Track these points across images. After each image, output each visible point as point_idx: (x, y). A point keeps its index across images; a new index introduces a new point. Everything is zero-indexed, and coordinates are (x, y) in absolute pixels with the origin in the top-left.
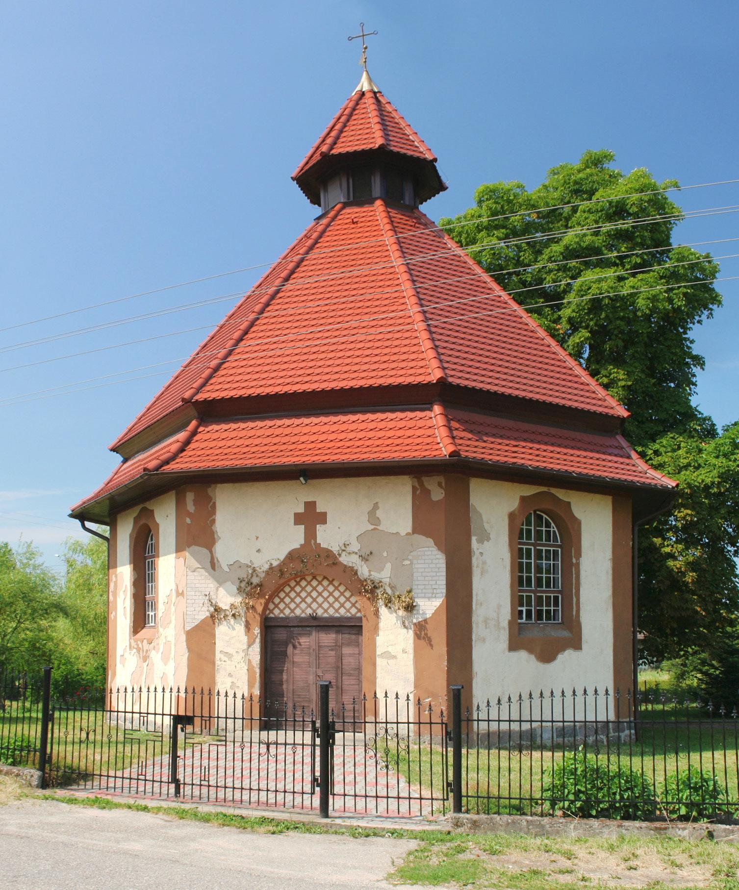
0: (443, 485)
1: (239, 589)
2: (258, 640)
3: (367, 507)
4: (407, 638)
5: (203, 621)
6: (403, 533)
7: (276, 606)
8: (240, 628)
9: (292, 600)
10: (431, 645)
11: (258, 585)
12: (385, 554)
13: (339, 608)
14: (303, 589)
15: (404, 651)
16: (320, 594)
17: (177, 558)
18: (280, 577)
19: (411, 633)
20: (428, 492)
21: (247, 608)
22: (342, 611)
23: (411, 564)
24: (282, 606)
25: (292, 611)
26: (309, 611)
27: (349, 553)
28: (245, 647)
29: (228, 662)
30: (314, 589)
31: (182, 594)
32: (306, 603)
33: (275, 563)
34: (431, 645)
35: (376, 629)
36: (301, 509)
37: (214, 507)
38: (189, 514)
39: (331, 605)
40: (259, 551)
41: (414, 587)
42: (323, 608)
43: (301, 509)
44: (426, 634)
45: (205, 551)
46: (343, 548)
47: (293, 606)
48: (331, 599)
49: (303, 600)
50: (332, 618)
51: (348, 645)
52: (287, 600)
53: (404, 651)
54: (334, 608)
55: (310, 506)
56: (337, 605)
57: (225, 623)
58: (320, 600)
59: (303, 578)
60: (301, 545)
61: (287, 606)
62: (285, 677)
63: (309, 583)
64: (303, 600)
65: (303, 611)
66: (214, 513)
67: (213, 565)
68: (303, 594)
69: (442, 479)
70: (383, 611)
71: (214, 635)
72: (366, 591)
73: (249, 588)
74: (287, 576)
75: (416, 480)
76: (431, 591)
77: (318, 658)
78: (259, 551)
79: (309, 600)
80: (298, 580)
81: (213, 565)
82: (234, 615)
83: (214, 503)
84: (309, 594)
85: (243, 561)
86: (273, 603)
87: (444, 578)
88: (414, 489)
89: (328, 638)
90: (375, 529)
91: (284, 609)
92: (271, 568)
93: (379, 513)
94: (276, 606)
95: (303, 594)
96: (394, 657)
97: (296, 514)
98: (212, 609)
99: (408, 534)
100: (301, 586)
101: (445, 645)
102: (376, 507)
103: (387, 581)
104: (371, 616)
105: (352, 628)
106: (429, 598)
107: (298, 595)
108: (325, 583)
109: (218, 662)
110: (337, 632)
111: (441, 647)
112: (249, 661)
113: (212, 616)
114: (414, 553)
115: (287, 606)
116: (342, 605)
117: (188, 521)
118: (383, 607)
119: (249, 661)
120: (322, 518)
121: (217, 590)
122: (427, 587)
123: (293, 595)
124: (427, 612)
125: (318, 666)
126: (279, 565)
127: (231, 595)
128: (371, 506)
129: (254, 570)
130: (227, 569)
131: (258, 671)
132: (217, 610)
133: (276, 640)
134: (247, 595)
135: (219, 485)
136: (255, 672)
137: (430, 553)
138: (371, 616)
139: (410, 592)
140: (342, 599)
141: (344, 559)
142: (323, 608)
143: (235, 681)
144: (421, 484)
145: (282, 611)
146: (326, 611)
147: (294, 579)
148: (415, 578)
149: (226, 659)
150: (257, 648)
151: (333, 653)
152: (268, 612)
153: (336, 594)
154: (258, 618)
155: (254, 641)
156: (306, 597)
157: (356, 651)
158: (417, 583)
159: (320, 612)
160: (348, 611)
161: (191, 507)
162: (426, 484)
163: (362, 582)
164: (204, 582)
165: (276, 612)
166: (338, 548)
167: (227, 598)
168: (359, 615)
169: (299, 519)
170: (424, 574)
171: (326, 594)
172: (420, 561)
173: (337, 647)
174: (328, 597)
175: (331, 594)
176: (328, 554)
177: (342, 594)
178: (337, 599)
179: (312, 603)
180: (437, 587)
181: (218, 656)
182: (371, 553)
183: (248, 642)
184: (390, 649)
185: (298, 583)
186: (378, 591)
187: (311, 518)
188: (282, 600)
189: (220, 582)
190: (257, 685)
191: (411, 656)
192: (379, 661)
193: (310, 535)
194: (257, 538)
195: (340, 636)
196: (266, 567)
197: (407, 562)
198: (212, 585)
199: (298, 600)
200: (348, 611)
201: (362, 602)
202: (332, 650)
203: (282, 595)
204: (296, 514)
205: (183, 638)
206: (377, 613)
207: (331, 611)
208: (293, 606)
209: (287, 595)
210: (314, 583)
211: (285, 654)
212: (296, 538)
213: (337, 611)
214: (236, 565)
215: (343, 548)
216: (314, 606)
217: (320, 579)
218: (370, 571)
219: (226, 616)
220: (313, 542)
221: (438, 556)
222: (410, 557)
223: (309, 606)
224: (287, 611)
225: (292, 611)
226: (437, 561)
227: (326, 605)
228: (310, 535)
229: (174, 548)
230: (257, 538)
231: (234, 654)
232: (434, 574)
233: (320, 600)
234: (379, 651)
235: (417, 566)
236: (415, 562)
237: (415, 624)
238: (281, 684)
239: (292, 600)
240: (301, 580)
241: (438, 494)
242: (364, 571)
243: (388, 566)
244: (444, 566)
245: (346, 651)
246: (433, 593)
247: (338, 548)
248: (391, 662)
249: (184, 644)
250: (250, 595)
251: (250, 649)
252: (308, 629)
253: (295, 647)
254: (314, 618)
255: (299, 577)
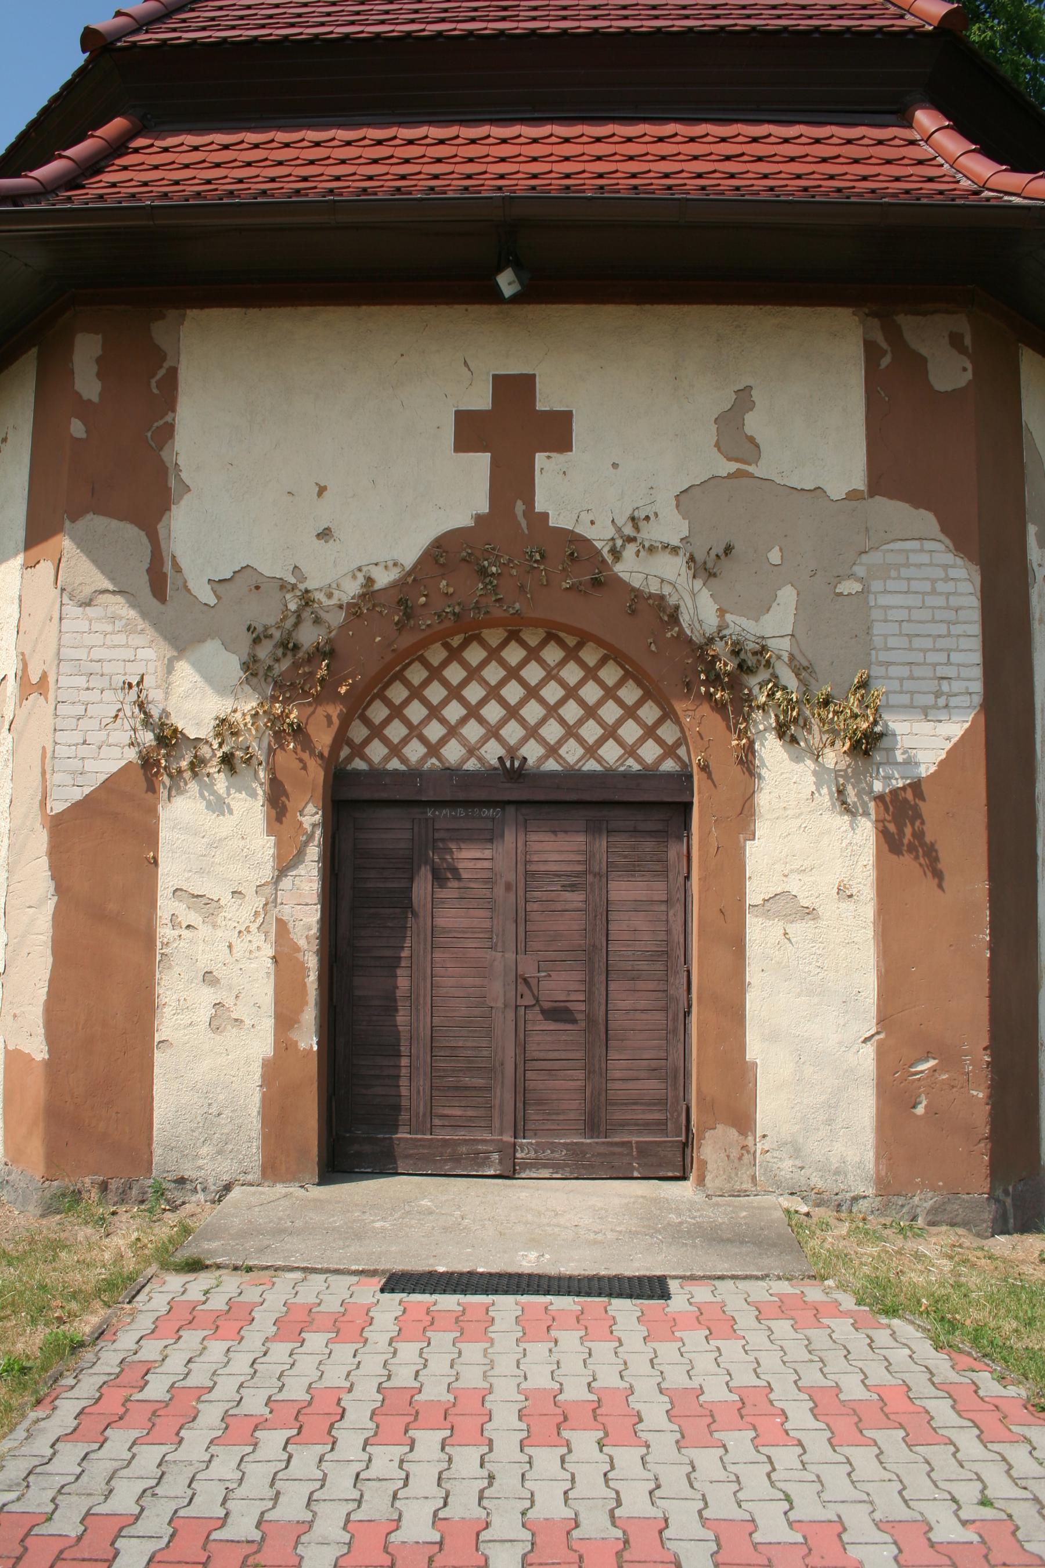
0: (968, 341)
1: (251, 668)
2: (313, 852)
3: (711, 399)
4: (851, 848)
5: (110, 784)
6: (837, 490)
7: (377, 732)
8: (249, 808)
9: (434, 712)
10: (938, 875)
11: (320, 652)
12: (775, 556)
13: (601, 742)
14: (473, 674)
15: (844, 893)
16: (532, 692)
17: (30, 565)
18: (400, 626)
19: (866, 831)
20: (914, 365)
21: (278, 735)
22: (611, 752)
23: (865, 592)
24: (396, 731)
25: (433, 750)
26: (492, 752)
27: (651, 549)
28: (267, 872)
29: (204, 930)
30: (513, 673)
31: (42, 686)
32: (481, 721)
33: (383, 579)
34: (938, 875)
35: (743, 815)
36: (481, 399)
37: (171, 382)
38: (84, 409)
39: (571, 732)
40: (325, 534)
41: (876, 671)
42: (542, 741)
43: (481, 399)
44: (919, 835)
45: (131, 532)
46: (629, 530)
47: (434, 731)
48: (571, 712)
49: (473, 712)
50: (572, 777)
51: (632, 869)
52: (416, 712)
53: (844, 893)
54: (581, 741)
55: (513, 390)
56: (591, 731)
57: (193, 787)
58: (532, 712)
59: (474, 638)
60: (479, 518)
61: (415, 731)
62: (403, 982)
63: (494, 654)
64: (473, 712)
65: (472, 751)
66: (170, 403)
67: (159, 581)
68: (474, 693)
69: (961, 324)
70: (771, 750)
71: (151, 838)
72: (715, 679)
73: (285, 664)
74: (426, 621)
75: (876, 322)
76: (933, 685)
77: (522, 918)
78: (325, 534)
79: (493, 712)
80: (456, 641)
81: (159, 581)
82: (227, 760)
83: (173, 373)
84: (494, 693)
85: (268, 569)
86: (367, 722)
87: (976, 644)
88: (872, 353)
89: (558, 849)
90: (739, 474)
91: (405, 741)
92: (369, 594)
93: (754, 423)
94: (377, 732)
95: (474, 693)
96: (810, 913)
97: (461, 417)
98: (148, 738)
99: (853, 495)
100: (464, 664)
101: (984, 873)
102: (744, 400)
103: (781, 646)
104: (727, 770)
105: (651, 812)
106: (925, 712)
107: (455, 693)
108: (552, 654)
109: (164, 932)
110: (593, 829)
111: (971, 884)
112: (282, 925)
113: (147, 763)
114: (874, 558)
115: (415, 731)
116: (611, 733)
117: (77, 428)
118: (771, 738)
119: (281, 924)
120: (557, 432)
121: (170, 669)
122: (918, 672)
123: (435, 693)
124: (921, 756)
125: (523, 947)
126: (393, 585)
127: (221, 690)
128: (725, 399)
129: (307, 600)
130: (207, 596)
131: (312, 962)
132: (169, 738)
133: (375, 848)
134: (278, 685)
135: (191, 313)
136: (303, 969)
137: (925, 558)
138: (727, 770)
139: (864, 685)
140: (611, 712)
141: (630, 569)
142: (542, 741)
143: (229, 1002)
144: (894, 334)
145: (395, 750)
146: (552, 751)
147: (442, 637)
148: (878, 641)
149: (193, 917)
150: (307, 880)
151: (576, 898)
152: (345, 752)
153: (591, 693)
154: (316, 773)
155: (301, 854)
156: (483, 702)
157: (658, 890)
158: (883, 656)
159: (532, 752)
160: (631, 751)
161: (87, 384)
162: (909, 336)
163: (700, 652)
164: (119, 642)
165: (376, 751)
166: (611, 532)
167: (201, 699)
168: (669, 765)
169: (470, 431)
170: (907, 628)
171: (552, 693)
172: (891, 585)
173: (587, 878)
174: (562, 702)
175: (571, 693)
176: (575, 548)
177: (610, 693)
178: (591, 712)
179: (503, 722)
180: (951, 672)
181: (166, 905)
182: (728, 550)
183: (279, 857)
184: (793, 886)
185: (455, 654)
186: (753, 681)
187: (514, 430)
188: (397, 712)
189: (181, 641)
190: (309, 1016)
191: (868, 911)
192: (759, 933)
193: (512, 483)
194: (322, 490)
195: (602, 843)
196: (352, 589)
197: (849, 587)
198: (149, 653)
199: (454, 712)
200: (631, 751)
201: (697, 717)
202: (573, 888)
203: (398, 693)
204: (461, 417)
205: (40, 840)
206: (747, 760)
207: (572, 752)
208: (434, 731)
209: (416, 693)
210: (514, 654)
211: (404, 903)
212: (459, 493)
213: (591, 751)
214: (246, 581)
215: (629, 530)
216: (512, 732)
217: (533, 642)
218: (722, 612)
219: (197, 764)
220: (520, 507)
221: (953, 573)
222: (860, 571)
223: (494, 732)
224: (415, 751)
225: (433, 750)
226: (950, 587)
227: (552, 731)
228: (512, 483)
229: (21, 534)
230: (322, 490)
231: (226, 899)
232: (942, 629)
233: (532, 712)
234: (755, 892)
235: (884, 600)
236: (876, 586)
237: (880, 798)
238: (390, 1008)
239: (434, 712)
240: (465, 644)
241: (950, 372)
242: (701, 611)
243: (787, 595)
244: (975, 602)
245: (624, 890)
246: (938, 694)
247: (611, 532)
248: (799, 929)
249: (41, 868)
250: (286, 688)
251: (286, 883)
252: (488, 812)
253: (439, 878)
254: (514, 772)
255: (464, 629)
